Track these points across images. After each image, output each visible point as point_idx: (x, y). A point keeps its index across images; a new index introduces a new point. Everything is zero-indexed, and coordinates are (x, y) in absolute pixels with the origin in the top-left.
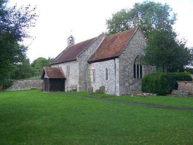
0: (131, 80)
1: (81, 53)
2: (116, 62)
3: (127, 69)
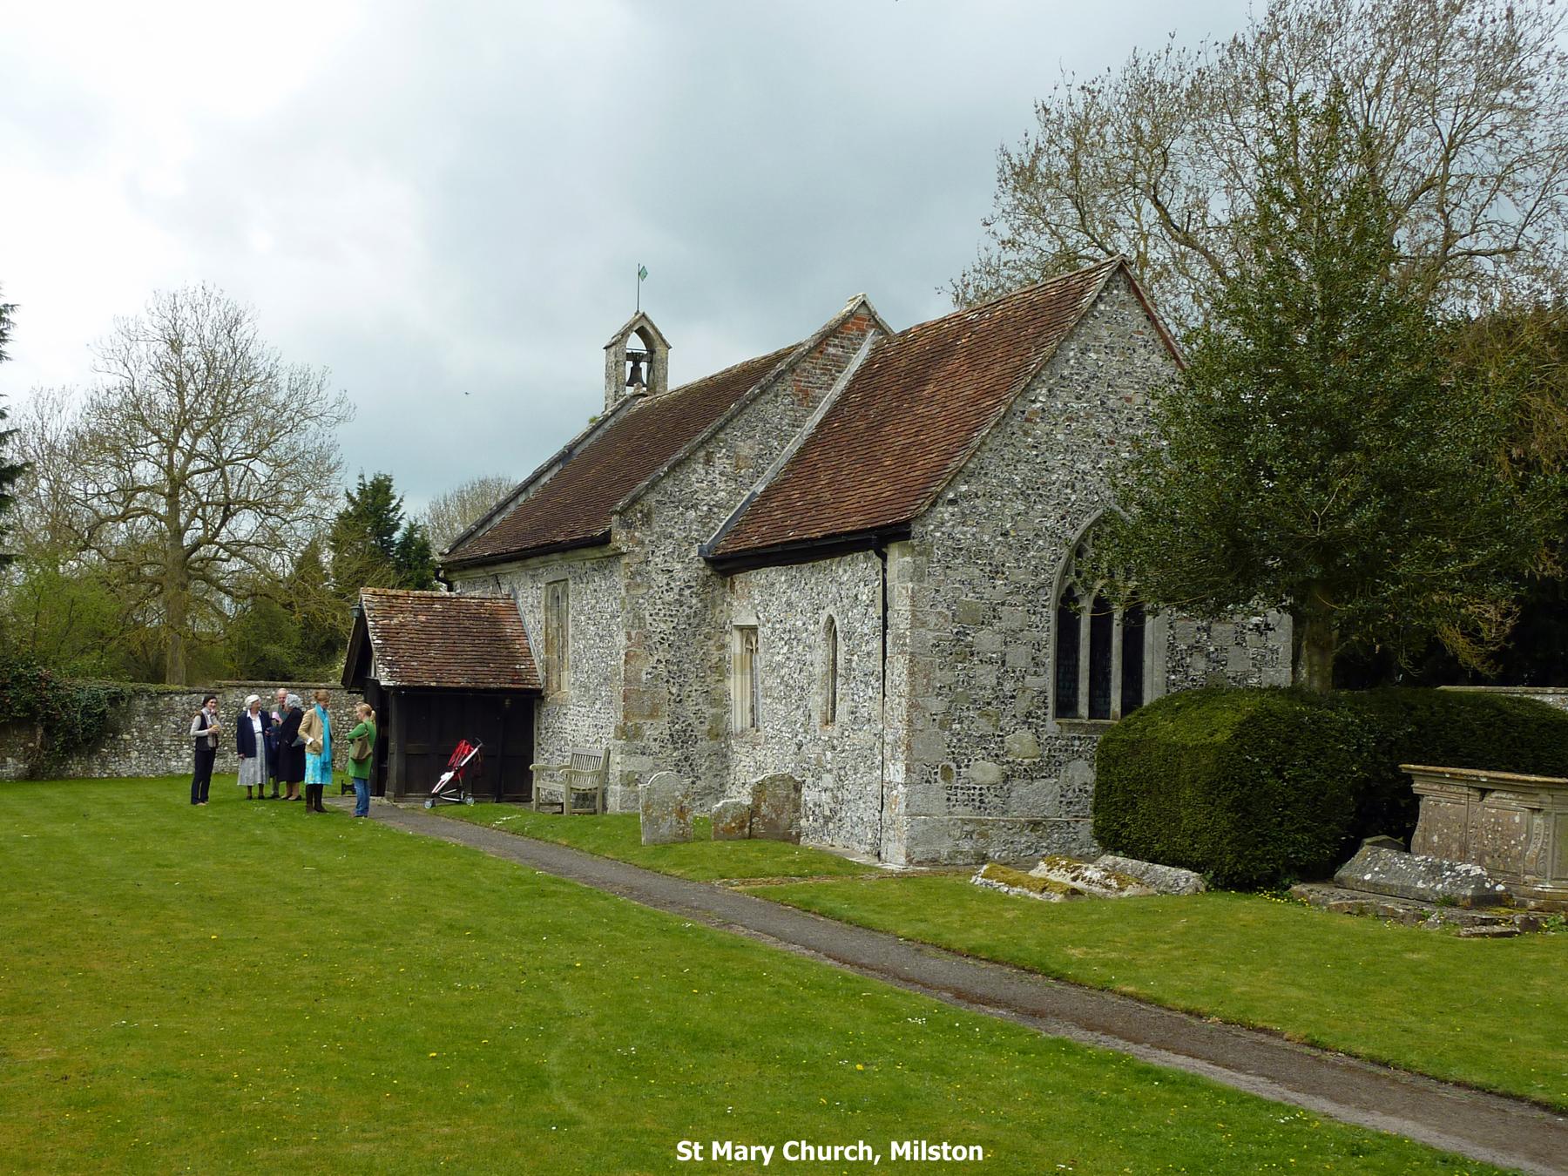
0: (1027, 735)
1: (652, 487)
2: (888, 577)
3: (986, 640)
